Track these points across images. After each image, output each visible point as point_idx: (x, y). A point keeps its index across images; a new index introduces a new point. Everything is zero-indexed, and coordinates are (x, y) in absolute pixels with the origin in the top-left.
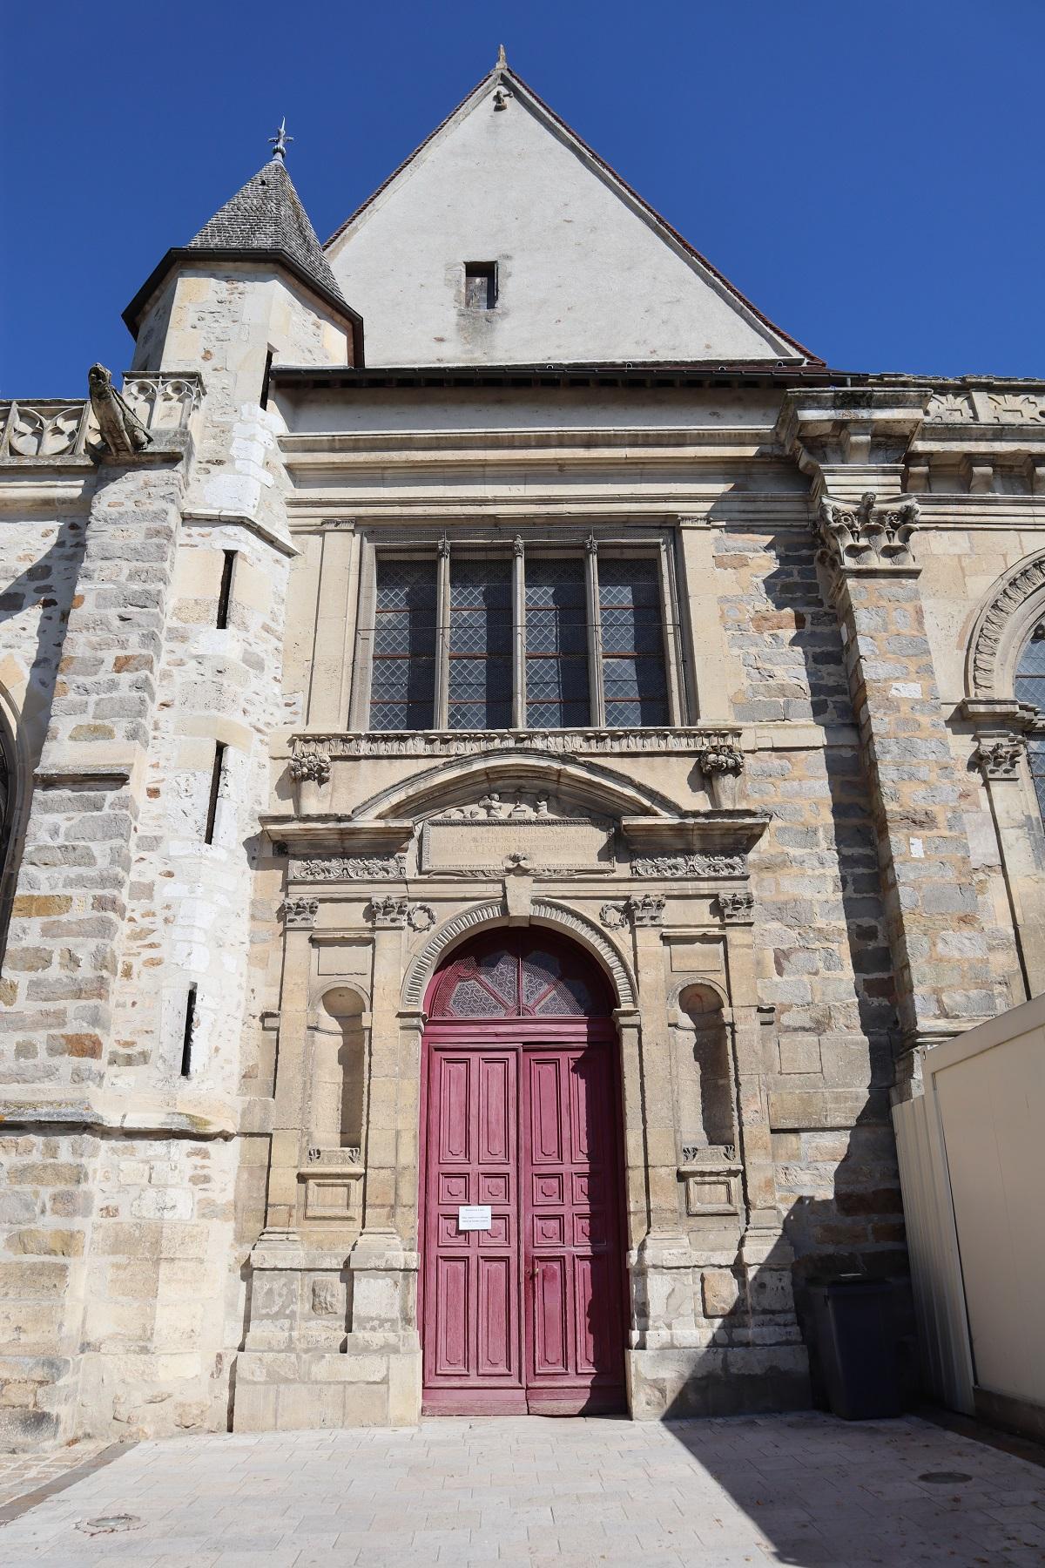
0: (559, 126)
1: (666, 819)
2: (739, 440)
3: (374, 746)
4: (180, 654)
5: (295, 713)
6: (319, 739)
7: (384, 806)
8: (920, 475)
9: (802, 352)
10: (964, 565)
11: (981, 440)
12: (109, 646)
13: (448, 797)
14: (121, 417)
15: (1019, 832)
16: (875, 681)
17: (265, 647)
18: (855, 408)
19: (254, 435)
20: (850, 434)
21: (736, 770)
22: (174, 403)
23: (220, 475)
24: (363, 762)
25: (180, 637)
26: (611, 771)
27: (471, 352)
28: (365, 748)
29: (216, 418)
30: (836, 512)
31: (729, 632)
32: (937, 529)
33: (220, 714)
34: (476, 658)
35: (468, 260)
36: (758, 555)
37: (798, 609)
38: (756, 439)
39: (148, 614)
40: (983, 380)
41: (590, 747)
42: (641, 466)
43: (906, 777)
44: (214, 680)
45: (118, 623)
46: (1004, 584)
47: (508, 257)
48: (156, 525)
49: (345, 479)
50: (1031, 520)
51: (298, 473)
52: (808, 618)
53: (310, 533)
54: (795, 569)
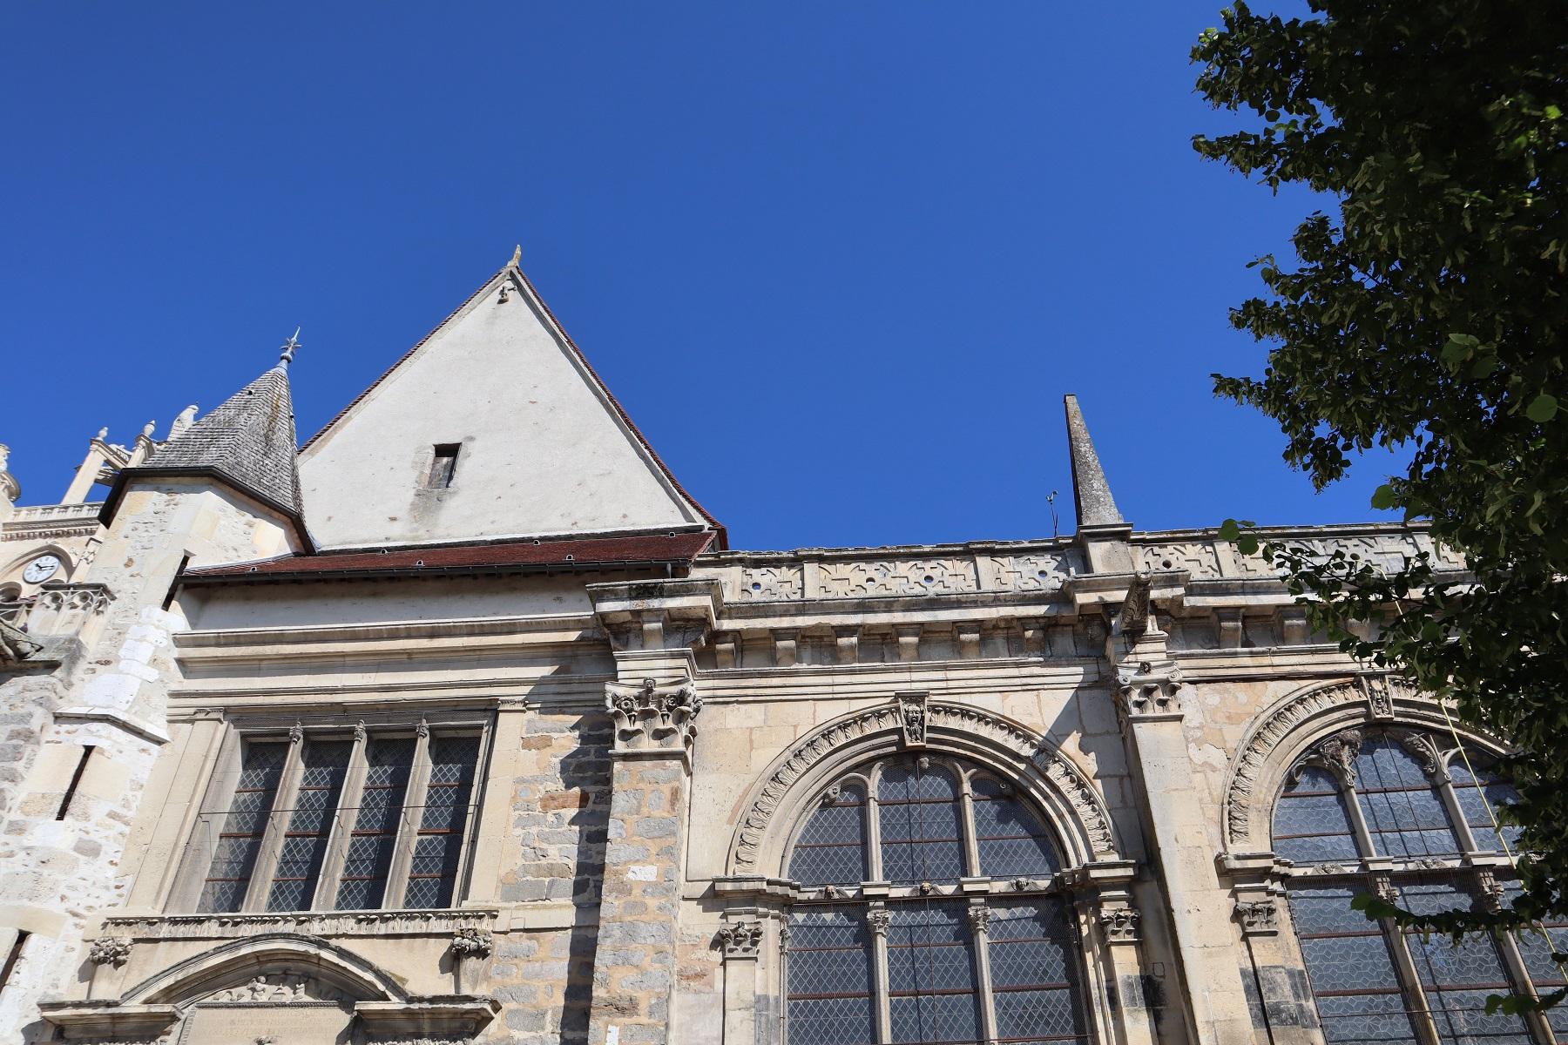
0: (546, 315)
1: (395, 1004)
2: (564, 626)
6: (128, 922)
7: (152, 991)
8: (726, 651)
9: (707, 518)
10: (753, 738)
11: (785, 615)
13: (221, 980)
15: (746, 1014)
16: (615, 865)
18: (649, 598)
20: (644, 622)
21: (482, 953)
22: (79, 611)
23: (105, 676)
24: (162, 943)
26: (356, 957)
27: (416, 530)
28: (165, 930)
29: (117, 621)
30: (615, 699)
31: (517, 812)
32: (738, 702)
33: (30, 904)
34: (309, 836)
35: (437, 443)
36: (562, 735)
37: (585, 788)
38: (578, 624)
40: (814, 553)
41: (359, 929)
42: (478, 653)
43: (620, 962)
44: (36, 870)
46: (789, 755)
47: (471, 439)
49: (227, 670)
50: (829, 689)
52: (592, 797)
53: (184, 721)
54: (592, 748)
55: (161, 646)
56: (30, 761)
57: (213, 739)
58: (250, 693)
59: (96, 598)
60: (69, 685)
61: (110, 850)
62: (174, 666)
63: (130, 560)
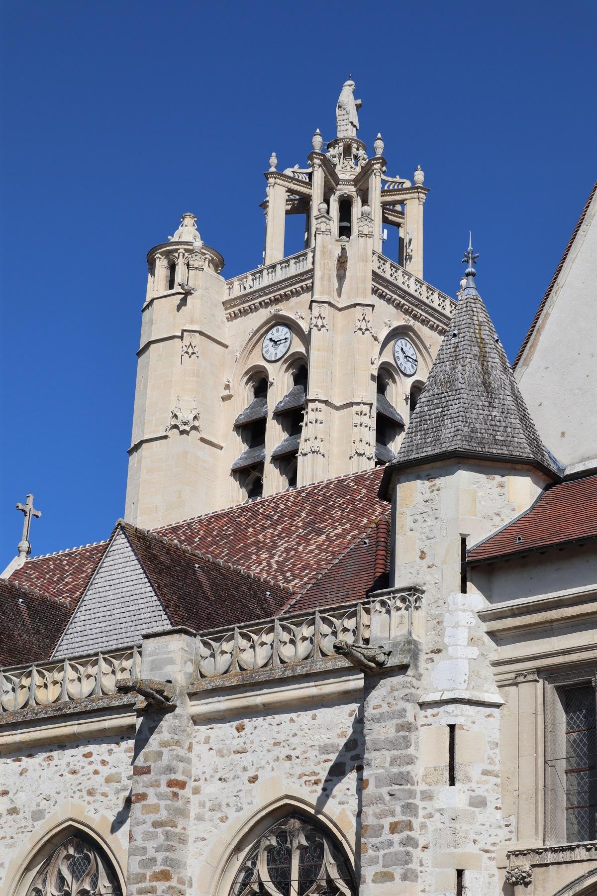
3: (556, 855)
4: (430, 810)
5: (511, 832)
6: (523, 853)
12: (385, 816)
14: (363, 658)
17: (487, 788)
19: (458, 622)
22: (403, 612)
25: (427, 796)
28: (550, 857)
33: (456, 850)
39: (403, 790)
44: (451, 826)
45: (388, 798)
48: (400, 721)
51: (497, 634)
55: (472, 625)
56: (417, 743)
57: (536, 698)
58: (552, 654)
59: (412, 599)
60: (419, 677)
61: (492, 800)
62: (487, 638)
63: (423, 552)
